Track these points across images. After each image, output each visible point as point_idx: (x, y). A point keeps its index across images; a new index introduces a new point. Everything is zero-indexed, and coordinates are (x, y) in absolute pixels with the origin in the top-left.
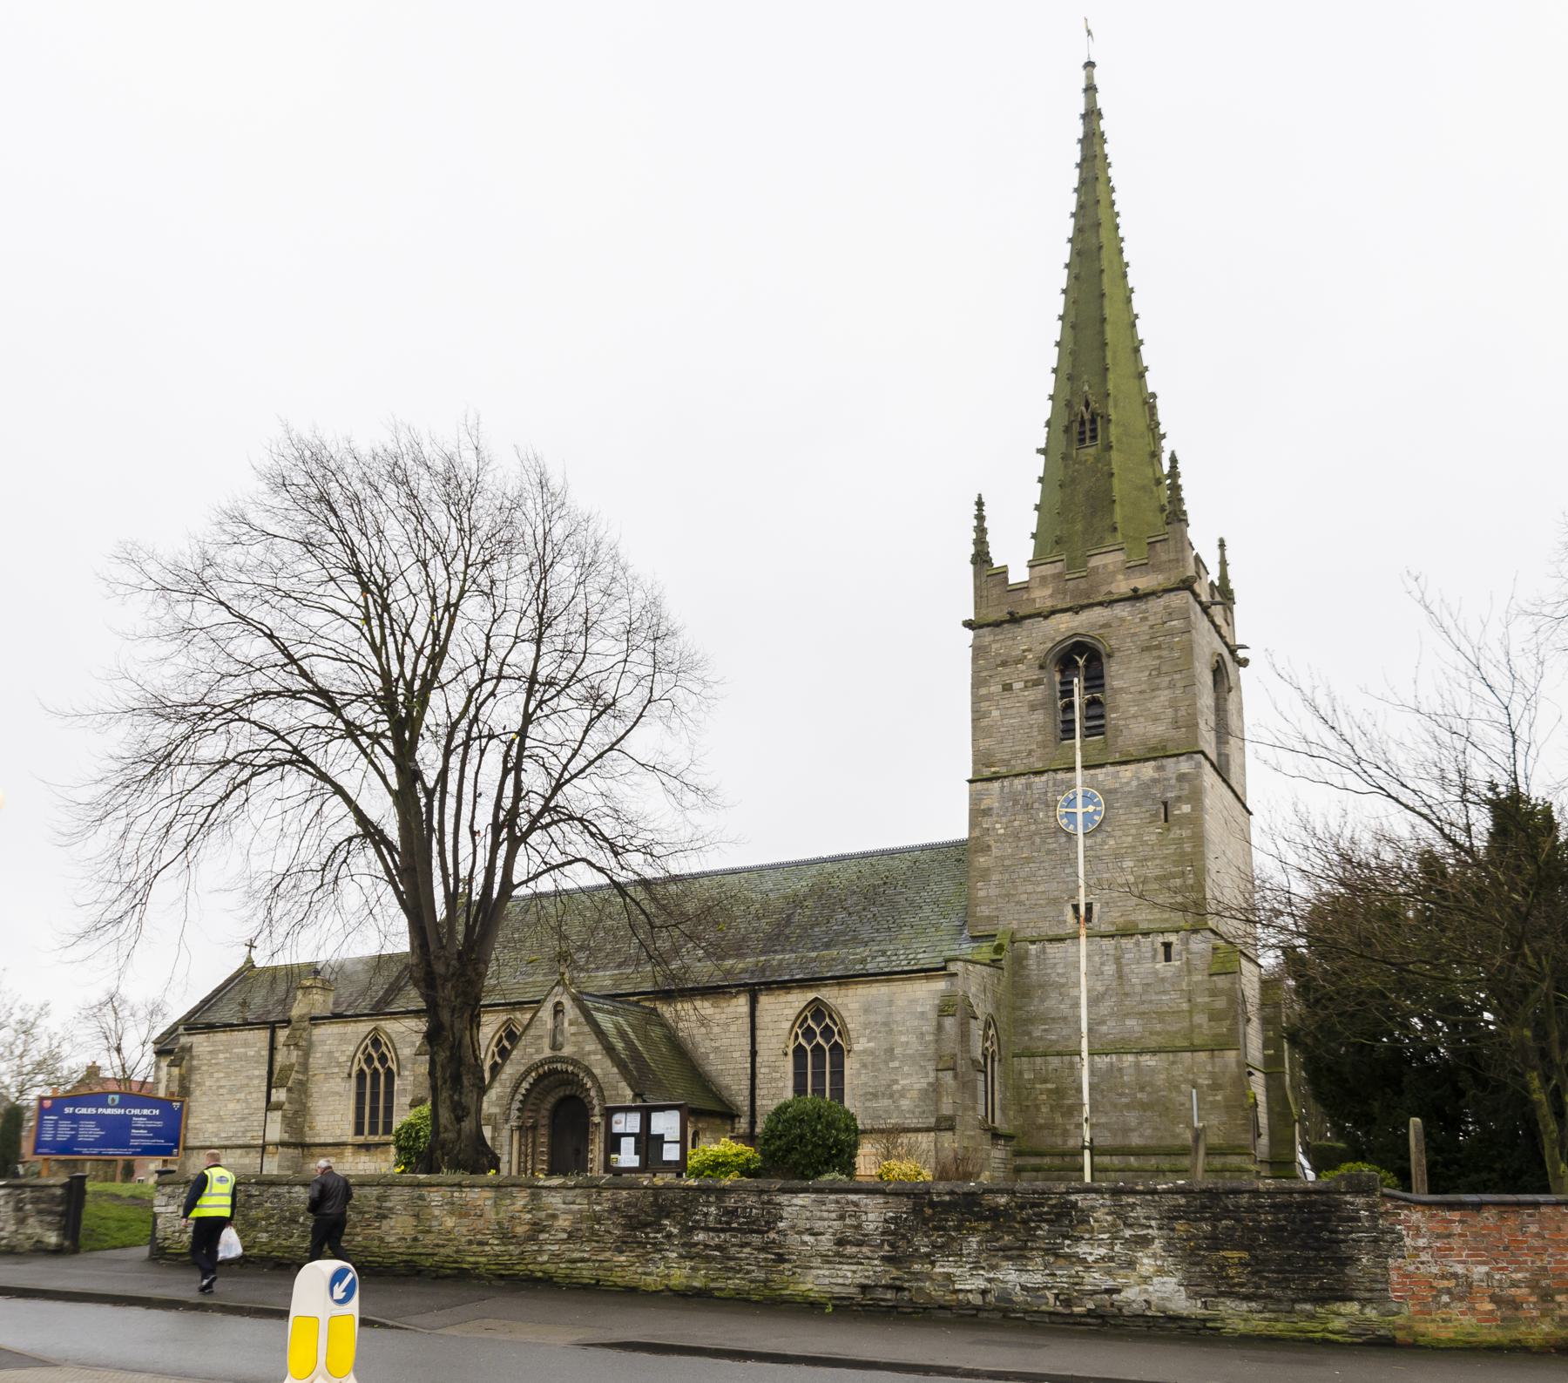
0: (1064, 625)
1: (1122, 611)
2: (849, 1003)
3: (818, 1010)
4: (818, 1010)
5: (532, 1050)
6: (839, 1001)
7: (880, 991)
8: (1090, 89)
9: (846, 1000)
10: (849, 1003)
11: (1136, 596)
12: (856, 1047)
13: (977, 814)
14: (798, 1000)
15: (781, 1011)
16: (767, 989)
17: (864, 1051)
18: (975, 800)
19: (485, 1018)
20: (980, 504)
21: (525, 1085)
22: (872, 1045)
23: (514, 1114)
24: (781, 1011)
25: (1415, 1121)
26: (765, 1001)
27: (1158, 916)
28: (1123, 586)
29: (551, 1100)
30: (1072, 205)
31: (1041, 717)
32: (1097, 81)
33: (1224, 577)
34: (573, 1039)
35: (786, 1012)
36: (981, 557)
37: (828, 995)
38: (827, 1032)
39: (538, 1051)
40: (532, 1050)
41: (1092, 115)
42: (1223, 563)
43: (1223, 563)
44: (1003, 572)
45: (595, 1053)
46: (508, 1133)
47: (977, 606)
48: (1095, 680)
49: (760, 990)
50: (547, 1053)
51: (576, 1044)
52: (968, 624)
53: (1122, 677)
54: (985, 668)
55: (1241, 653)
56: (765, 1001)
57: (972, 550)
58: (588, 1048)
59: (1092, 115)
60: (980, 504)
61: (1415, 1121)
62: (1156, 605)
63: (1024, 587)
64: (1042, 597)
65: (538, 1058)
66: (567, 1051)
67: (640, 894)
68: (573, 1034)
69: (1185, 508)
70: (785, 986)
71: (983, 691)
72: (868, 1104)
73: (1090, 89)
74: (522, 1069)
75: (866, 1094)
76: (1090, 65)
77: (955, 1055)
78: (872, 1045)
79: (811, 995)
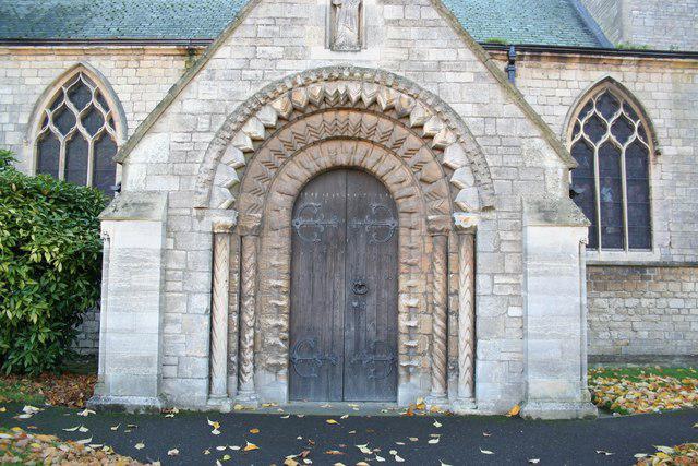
3: (609, 97)
5: (276, 51)
6: (639, 87)
9: (649, 87)
12: (667, 150)
16: (532, 57)
17: (680, 156)
21: (255, 128)
22: (688, 149)
23: (222, 198)
25: (169, 453)
29: (297, 171)
34: (393, 32)
35: (559, 93)
37: (627, 75)
39: (291, 53)
40: (276, 51)
45: (458, 68)
46: (207, 242)
49: (521, 58)
50: (320, 56)
51: (400, 43)
58: (433, 56)
61: (169, 453)
65: (293, 67)
66: (375, 56)
68: (389, 22)
69: (22, 12)
72: (687, 228)
74: (248, 92)
75: (685, 213)
78: (688, 149)
79: (598, 74)
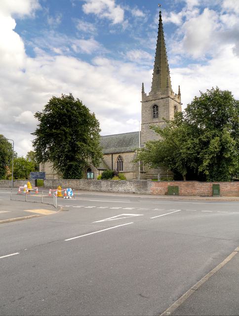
0: (153, 102)
1: (161, 100)
2: (123, 155)
3: (120, 157)
4: (120, 157)
7: (127, 154)
10: (123, 155)
11: (162, 98)
13: (142, 129)
14: (117, 155)
15: (116, 157)
18: (142, 127)
20: (143, 84)
24: (116, 157)
26: (114, 155)
27: (155, 124)
28: (161, 96)
31: (80, 25)
36: (143, 92)
37: (121, 155)
47: (142, 99)
48: (157, 110)
53: (161, 110)
54: (143, 108)
56: (114, 155)
60: (143, 84)
62: (165, 100)
63: (148, 96)
64: (151, 98)
67: (151, 94)
70: (116, 153)
76: (160, 12)
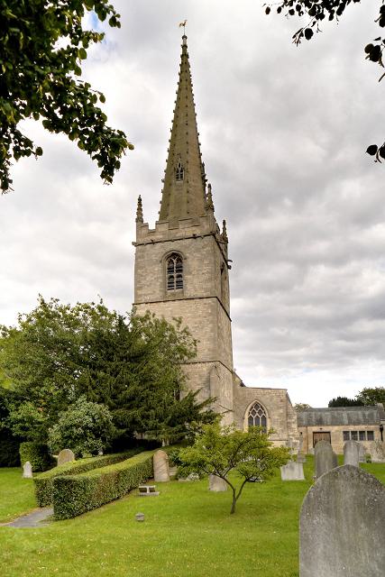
8: (184, 47)
19: (32, 543)
20: (140, 200)
30: (175, 99)
32: (187, 44)
33: (224, 233)
36: (139, 219)
38: (260, 412)
41: (185, 56)
42: (224, 229)
43: (224, 229)
44: (147, 225)
52: (133, 243)
55: (229, 263)
57: (136, 216)
59: (185, 56)
60: (140, 200)
71: (140, 292)
73: (184, 47)
77: (346, 433)
